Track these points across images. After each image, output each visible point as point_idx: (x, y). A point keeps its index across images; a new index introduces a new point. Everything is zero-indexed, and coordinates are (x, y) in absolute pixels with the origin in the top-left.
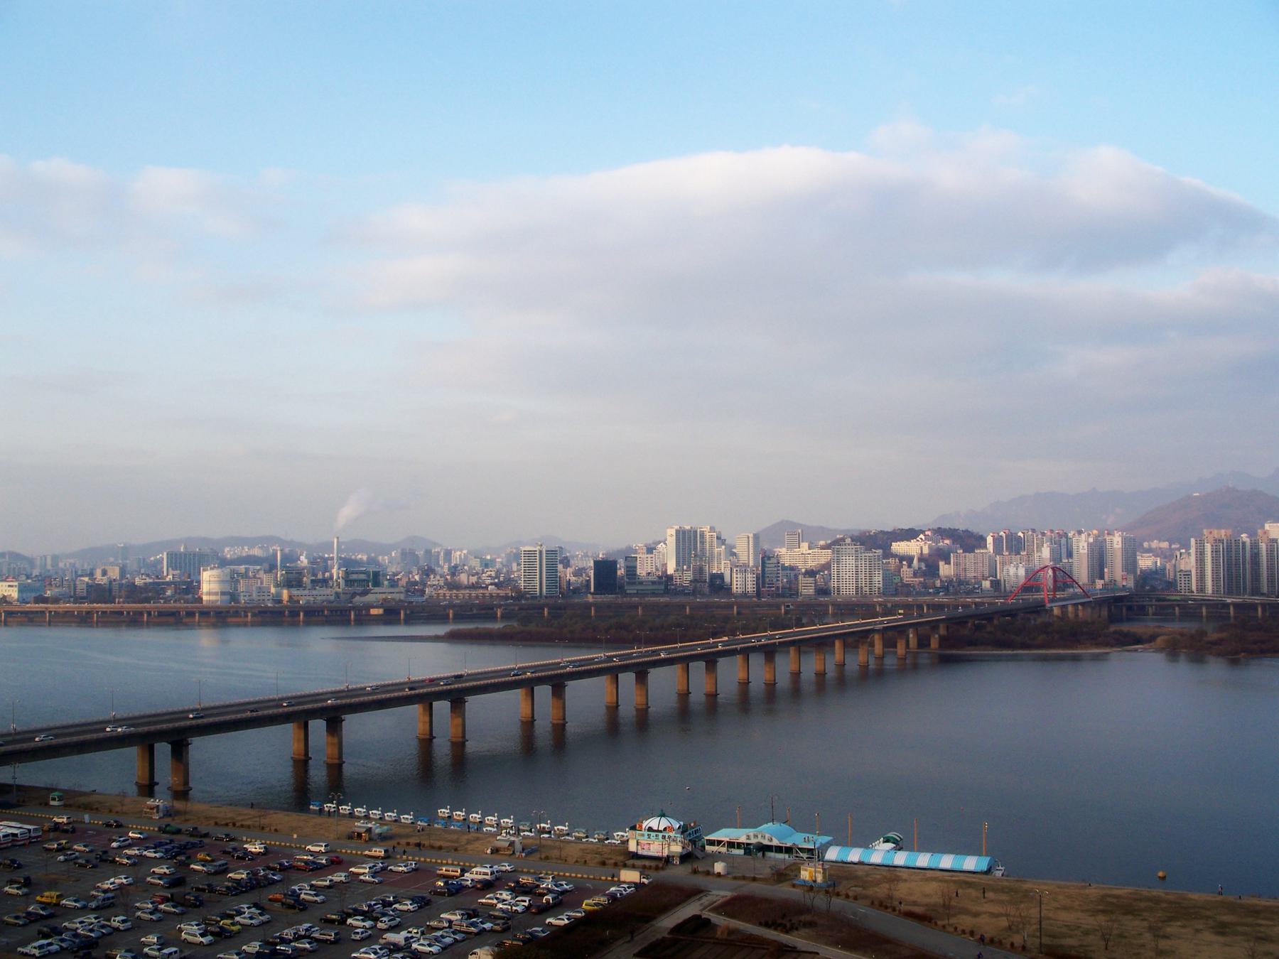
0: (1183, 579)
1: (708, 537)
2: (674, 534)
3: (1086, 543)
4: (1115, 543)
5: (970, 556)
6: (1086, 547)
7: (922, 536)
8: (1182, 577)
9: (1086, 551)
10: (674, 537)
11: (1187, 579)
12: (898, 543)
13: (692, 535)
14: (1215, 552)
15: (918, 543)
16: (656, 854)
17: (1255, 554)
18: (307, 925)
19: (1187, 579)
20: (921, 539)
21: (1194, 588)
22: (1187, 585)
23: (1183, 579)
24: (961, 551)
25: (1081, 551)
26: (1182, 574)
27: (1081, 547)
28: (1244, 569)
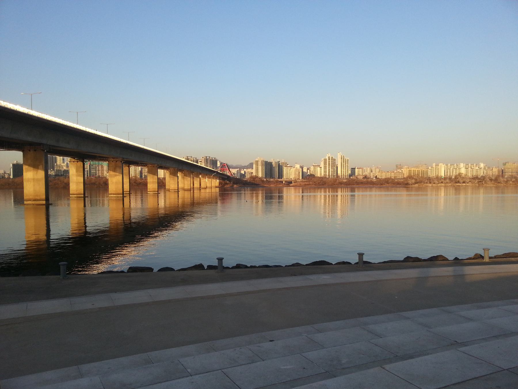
0: (248, 175)
23: (248, 175)
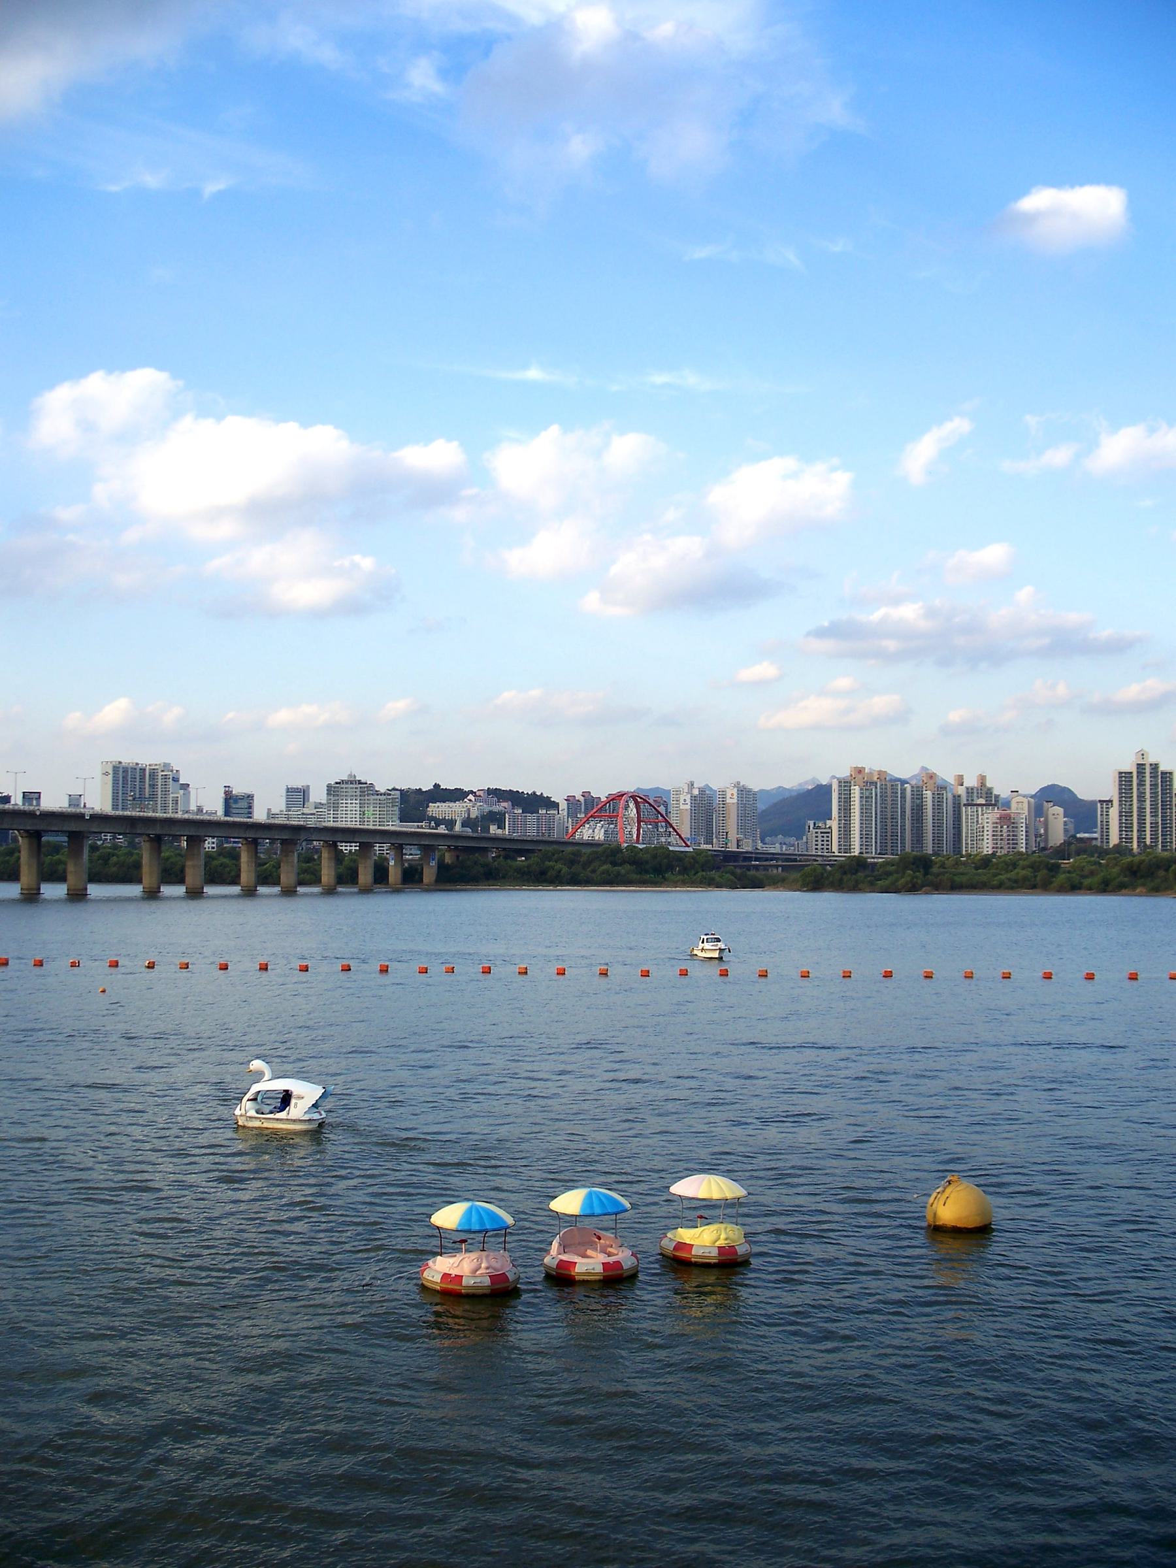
0: (820, 839)
1: (160, 777)
2: (111, 772)
3: (736, 789)
4: (728, 795)
5: (531, 817)
6: (688, 801)
7: (471, 797)
8: (820, 835)
9: (688, 807)
10: (110, 777)
11: (825, 839)
12: (438, 804)
13: (138, 774)
14: (865, 799)
15: (465, 805)
16: (350, 825)
17: (917, 806)
18: (994, 554)
19: (825, 839)
20: (470, 800)
21: (835, 848)
22: (825, 843)
23: (820, 839)
24: (520, 811)
25: (682, 807)
26: (819, 831)
27: (682, 801)
28: (903, 826)
